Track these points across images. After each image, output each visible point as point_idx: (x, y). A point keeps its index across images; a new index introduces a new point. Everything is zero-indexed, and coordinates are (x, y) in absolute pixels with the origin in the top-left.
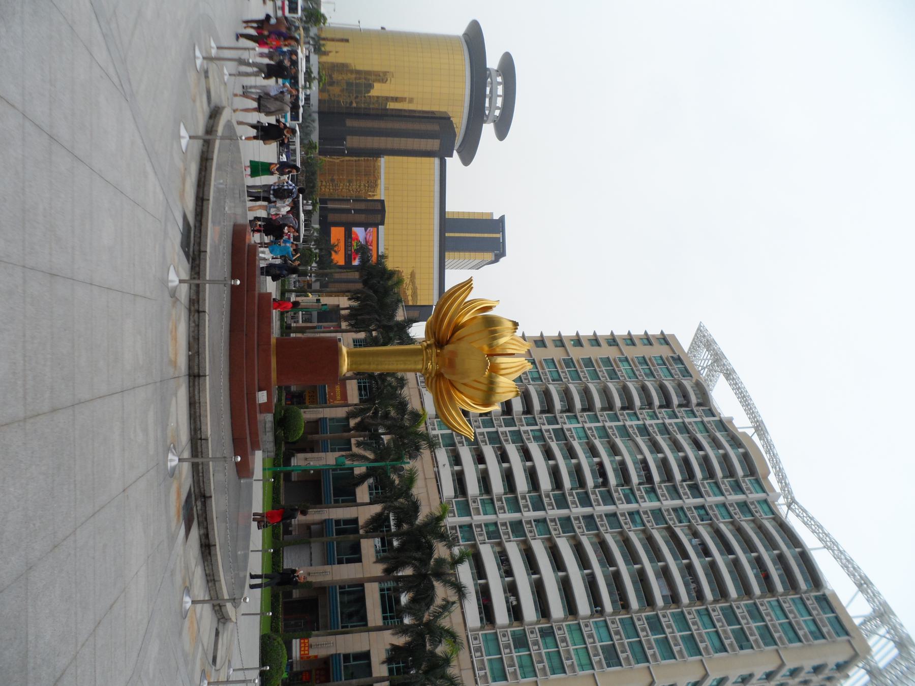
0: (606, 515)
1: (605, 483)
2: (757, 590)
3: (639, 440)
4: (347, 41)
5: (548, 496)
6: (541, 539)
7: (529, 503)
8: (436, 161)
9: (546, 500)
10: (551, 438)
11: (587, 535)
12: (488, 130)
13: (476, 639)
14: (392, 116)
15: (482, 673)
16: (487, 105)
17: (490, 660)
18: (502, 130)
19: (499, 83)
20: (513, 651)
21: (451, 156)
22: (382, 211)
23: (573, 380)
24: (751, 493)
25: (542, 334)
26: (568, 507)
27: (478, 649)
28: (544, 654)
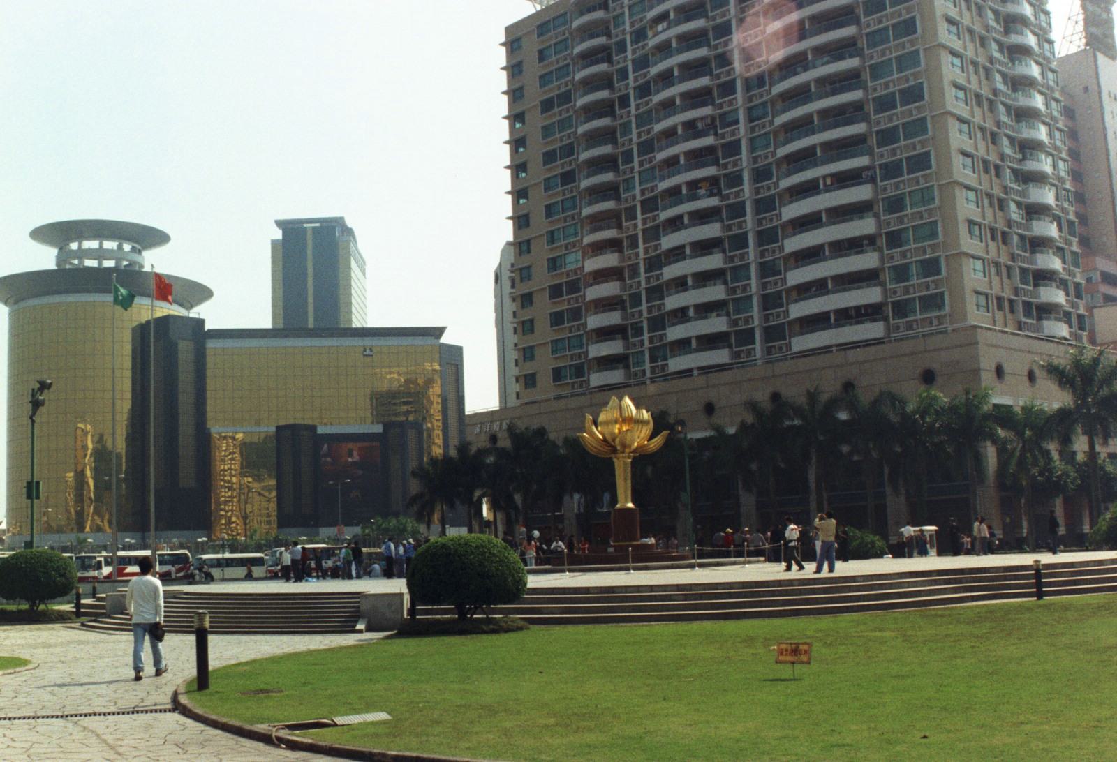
0: (765, 309)
1: (710, 150)
2: (862, 161)
3: (657, 98)
5: (729, 228)
6: (780, 207)
7: (726, 99)
8: (211, 344)
9: (735, 231)
10: (647, 103)
11: (778, 180)
12: (154, 261)
13: (892, 258)
15: (922, 180)
20: (911, 283)
22: (293, 428)
23: (568, 74)
24: (728, 10)
25: (503, 69)
26: (739, 140)
28: (922, 317)
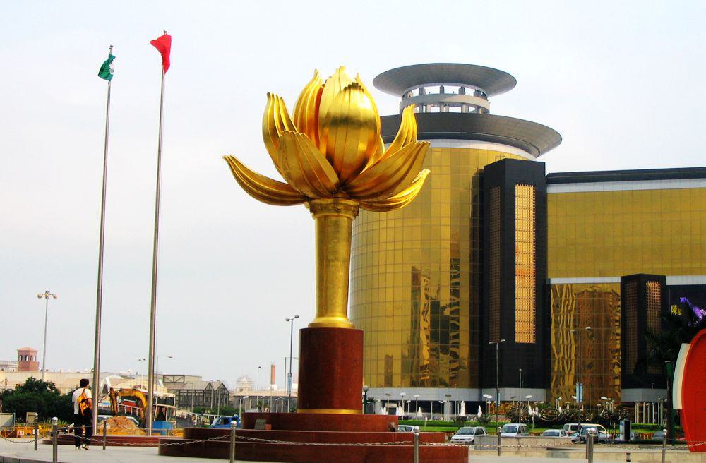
4: (273, 367)
12: (499, 105)
14: (481, 267)
16: (457, 110)
17: (153, 432)
18: (491, 80)
19: (422, 90)
21: (542, 165)
27: (188, 393)
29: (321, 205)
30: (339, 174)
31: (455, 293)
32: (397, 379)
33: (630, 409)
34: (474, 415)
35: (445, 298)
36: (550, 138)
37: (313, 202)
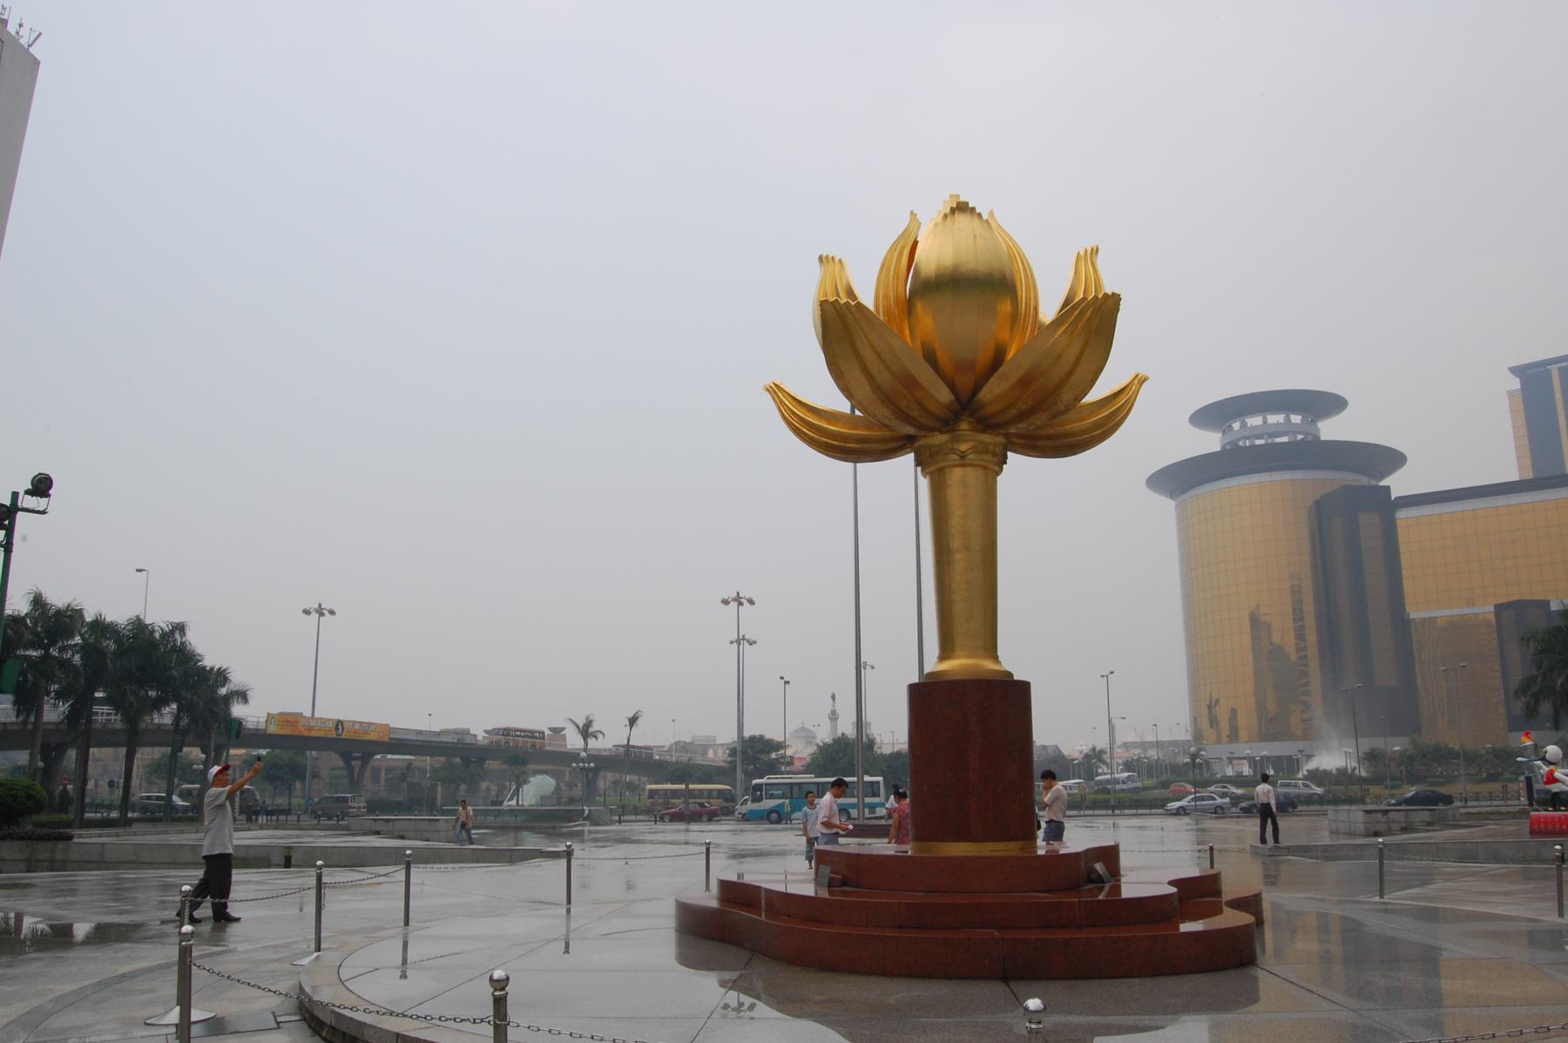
12: (1331, 429)
29: (930, 447)
30: (952, 387)
31: (1300, 635)
32: (1243, 734)
33: (893, 831)
34: (861, 822)
35: (1289, 642)
36: (1393, 459)
37: (918, 444)
